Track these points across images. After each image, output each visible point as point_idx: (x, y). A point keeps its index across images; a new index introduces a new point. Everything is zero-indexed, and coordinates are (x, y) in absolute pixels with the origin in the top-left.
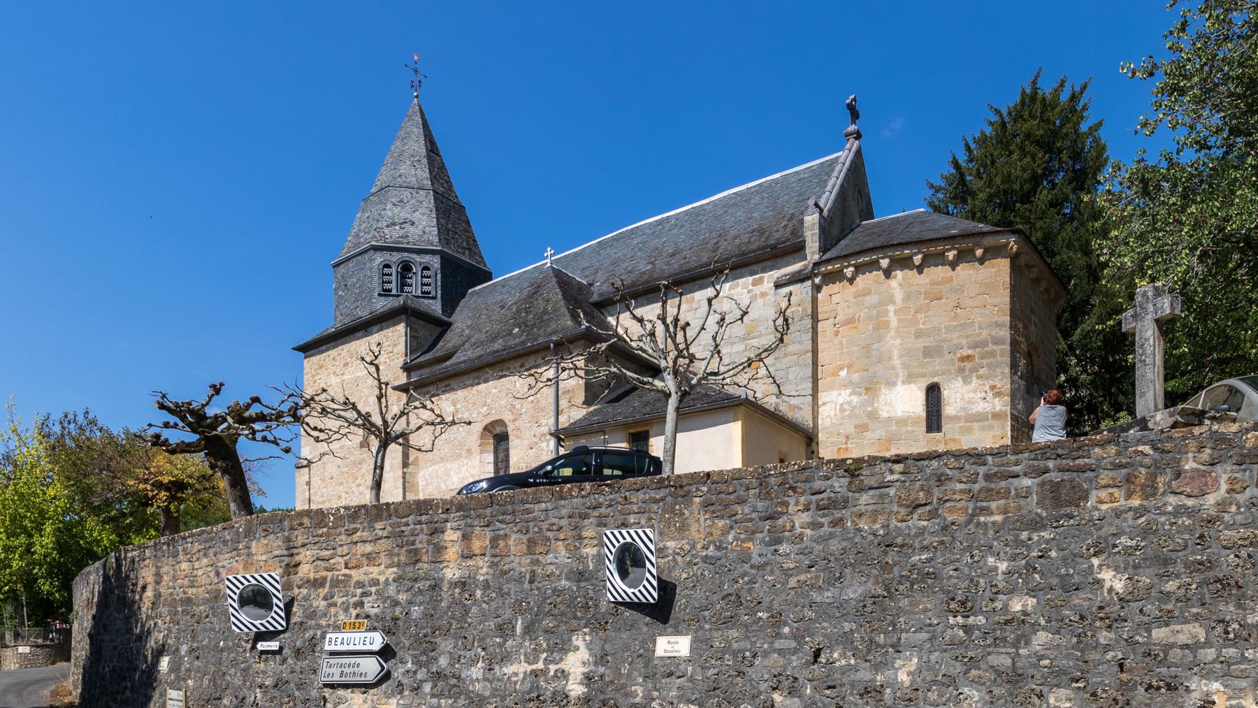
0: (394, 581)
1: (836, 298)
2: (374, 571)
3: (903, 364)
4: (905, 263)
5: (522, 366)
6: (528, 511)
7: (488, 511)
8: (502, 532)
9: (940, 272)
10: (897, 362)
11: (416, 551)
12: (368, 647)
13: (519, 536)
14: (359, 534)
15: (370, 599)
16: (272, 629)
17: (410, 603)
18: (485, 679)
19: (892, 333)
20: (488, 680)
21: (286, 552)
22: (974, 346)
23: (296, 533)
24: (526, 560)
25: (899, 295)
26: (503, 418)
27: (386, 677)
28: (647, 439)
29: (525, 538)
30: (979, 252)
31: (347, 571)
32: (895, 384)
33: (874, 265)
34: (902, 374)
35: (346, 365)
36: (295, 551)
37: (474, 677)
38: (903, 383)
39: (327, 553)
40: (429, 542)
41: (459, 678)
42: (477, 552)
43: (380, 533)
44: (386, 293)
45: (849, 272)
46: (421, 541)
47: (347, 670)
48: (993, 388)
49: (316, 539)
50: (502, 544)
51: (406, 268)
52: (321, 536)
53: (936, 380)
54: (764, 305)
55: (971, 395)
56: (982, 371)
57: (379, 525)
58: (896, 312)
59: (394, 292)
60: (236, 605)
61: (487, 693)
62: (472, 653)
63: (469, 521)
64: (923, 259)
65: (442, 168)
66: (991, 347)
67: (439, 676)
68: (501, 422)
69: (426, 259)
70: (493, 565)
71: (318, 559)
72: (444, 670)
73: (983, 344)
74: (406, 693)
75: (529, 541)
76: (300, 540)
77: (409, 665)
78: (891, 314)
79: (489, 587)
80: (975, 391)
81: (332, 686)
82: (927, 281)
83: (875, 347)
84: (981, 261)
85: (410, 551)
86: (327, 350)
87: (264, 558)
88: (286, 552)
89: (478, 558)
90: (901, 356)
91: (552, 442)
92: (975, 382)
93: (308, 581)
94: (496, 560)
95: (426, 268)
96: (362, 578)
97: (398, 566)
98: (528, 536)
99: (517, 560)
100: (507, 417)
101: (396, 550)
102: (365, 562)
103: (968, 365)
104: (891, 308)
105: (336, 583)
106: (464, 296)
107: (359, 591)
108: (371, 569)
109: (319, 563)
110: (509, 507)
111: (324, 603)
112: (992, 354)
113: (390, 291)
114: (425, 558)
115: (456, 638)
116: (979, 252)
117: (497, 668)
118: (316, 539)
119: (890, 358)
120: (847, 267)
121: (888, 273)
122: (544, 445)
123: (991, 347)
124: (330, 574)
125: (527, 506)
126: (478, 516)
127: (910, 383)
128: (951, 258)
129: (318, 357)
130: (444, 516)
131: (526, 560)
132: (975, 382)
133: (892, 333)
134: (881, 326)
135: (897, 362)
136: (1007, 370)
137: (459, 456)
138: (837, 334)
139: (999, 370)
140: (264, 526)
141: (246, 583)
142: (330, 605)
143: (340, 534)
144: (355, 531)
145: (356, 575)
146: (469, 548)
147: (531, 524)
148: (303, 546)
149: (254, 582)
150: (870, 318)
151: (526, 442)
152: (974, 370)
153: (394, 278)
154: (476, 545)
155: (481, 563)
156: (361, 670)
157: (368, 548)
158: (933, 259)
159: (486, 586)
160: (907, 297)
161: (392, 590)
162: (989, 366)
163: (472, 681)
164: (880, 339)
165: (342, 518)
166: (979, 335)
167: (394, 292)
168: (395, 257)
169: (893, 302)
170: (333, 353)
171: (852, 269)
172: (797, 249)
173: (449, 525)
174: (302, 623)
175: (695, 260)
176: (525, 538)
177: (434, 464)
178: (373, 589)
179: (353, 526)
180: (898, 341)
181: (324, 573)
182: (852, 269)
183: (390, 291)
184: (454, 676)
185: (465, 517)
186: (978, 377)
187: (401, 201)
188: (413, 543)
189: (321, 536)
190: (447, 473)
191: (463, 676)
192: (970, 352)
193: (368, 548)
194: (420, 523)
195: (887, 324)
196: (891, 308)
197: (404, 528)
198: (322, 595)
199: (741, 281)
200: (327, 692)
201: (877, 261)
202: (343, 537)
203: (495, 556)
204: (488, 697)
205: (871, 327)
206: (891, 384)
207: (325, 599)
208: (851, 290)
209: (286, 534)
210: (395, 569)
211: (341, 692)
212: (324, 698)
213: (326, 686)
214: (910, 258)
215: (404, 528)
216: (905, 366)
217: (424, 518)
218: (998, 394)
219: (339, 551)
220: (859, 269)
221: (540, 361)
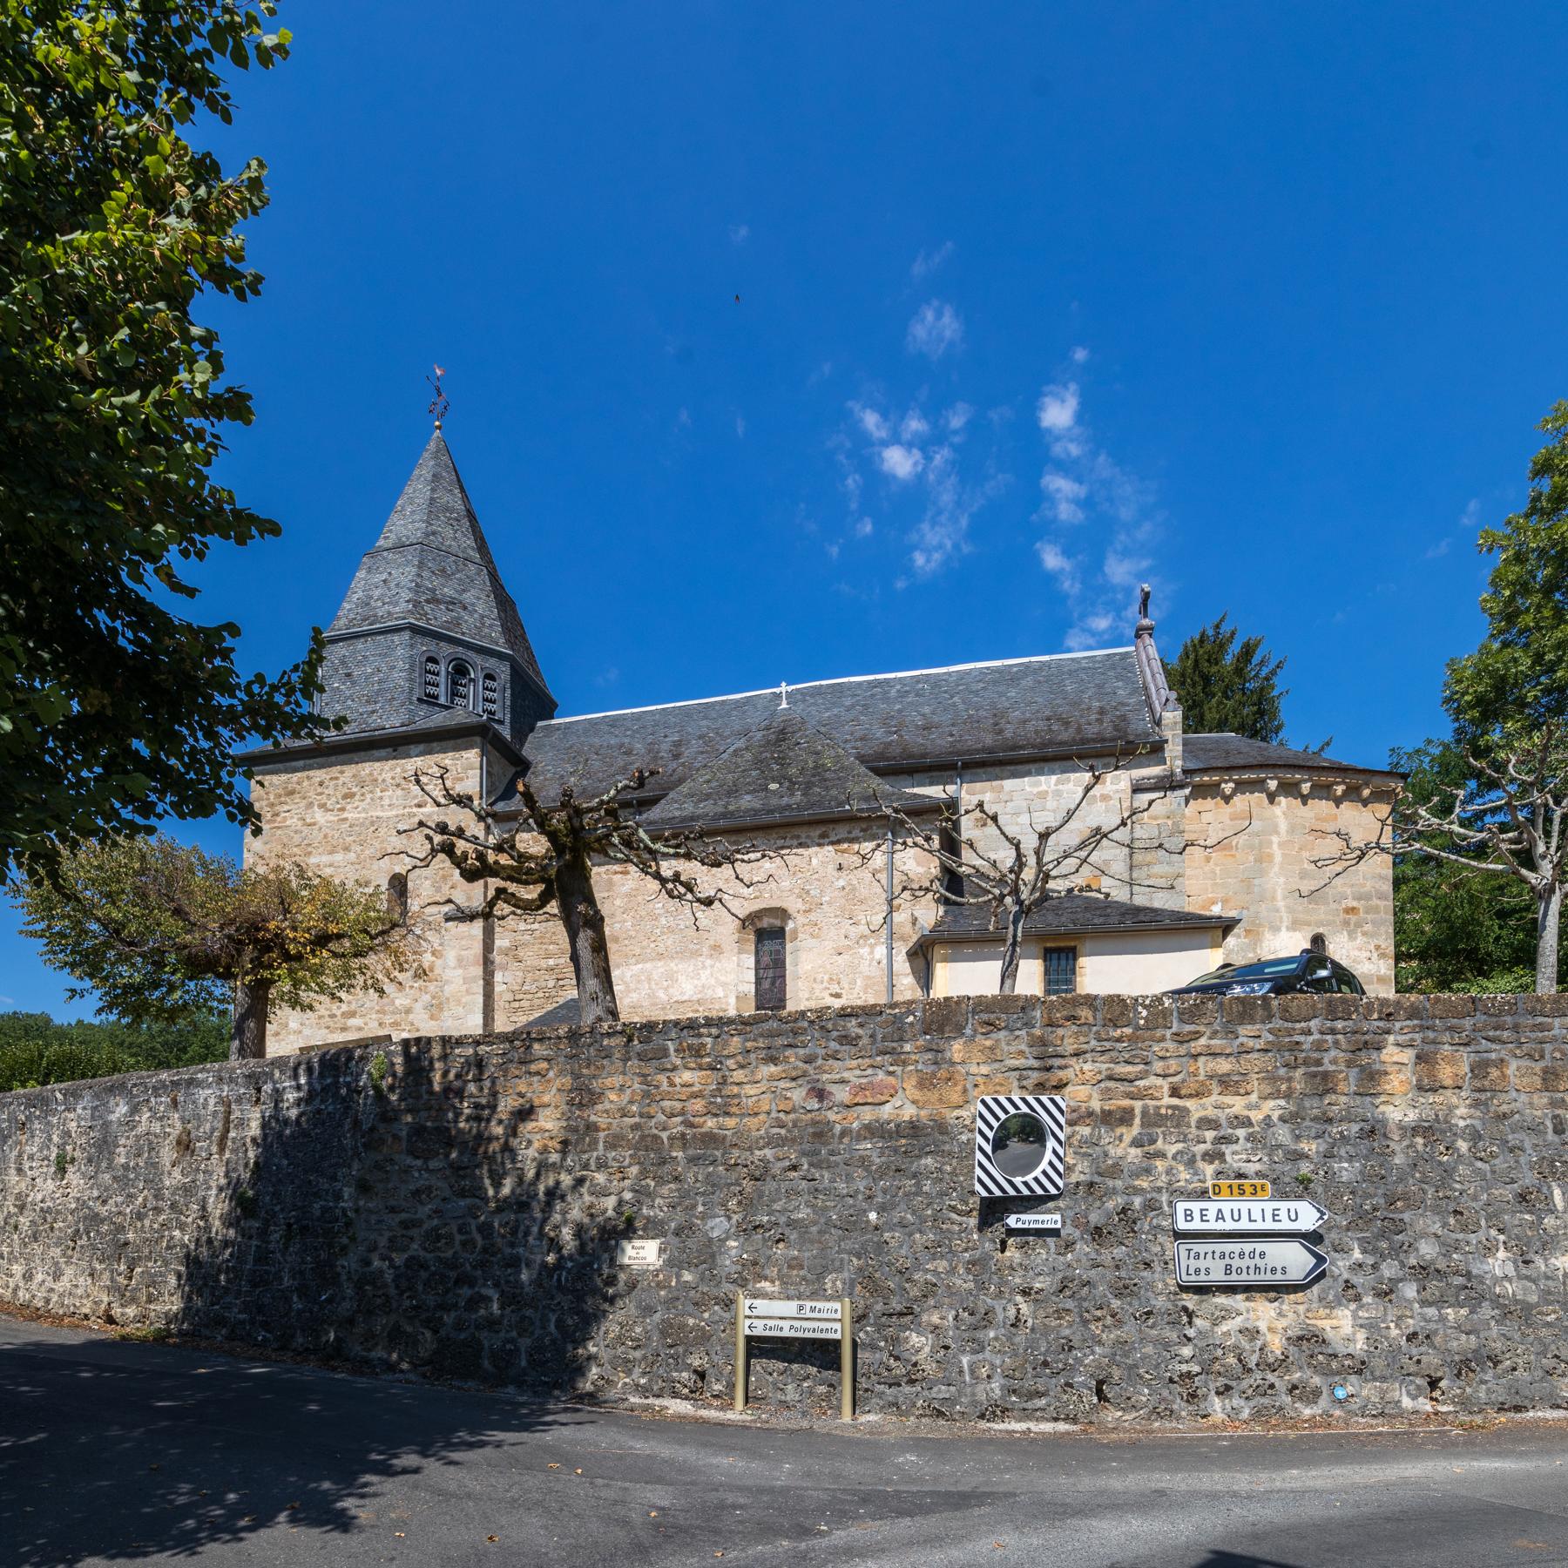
0: (1282, 1119)
1: (1206, 817)
2: (1237, 1105)
3: (1287, 907)
4: (1289, 789)
5: (823, 836)
6: (1542, 1028)
7: (1468, 1023)
8: (1493, 1056)
9: (1323, 807)
10: (1281, 904)
11: (1326, 1076)
12: (1286, 1225)
13: (1526, 1063)
14: (1203, 1041)
15: (1235, 1147)
16: (1040, 1192)
17: (1329, 1155)
18: (1520, 1277)
19: (1276, 869)
20: (1527, 1278)
21: (1036, 1063)
22: (1359, 899)
23: (1060, 1032)
24: (1542, 1100)
25: (1283, 826)
26: (784, 905)
27: (1318, 1276)
28: (1075, 959)
29: (1538, 1067)
30: (1366, 792)
31: (1175, 1101)
32: (1278, 929)
33: (1259, 785)
34: (1286, 919)
35: (349, 796)
36: (1057, 1062)
37: (1499, 1273)
38: (1288, 929)
39: (1129, 1068)
40: (1349, 1064)
41: (1468, 1275)
42: (1448, 1082)
43: (1251, 1043)
44: (430, 700)
45: (1228, 788)
46: (1333, 1060)
47: (1236, 1263)
48: (1378, 947)
49: (1108, 1045)
50: (1494, 1073)
51: (460, 670)
52: (1119, 1040)
53: (1321, 930)
54: (1107, 811)
55: (1357, 953)
56: (1367, 927)
57: (1245, 1030)
58: (1280, 845)
59: (442, 700)
60: (988, 1149)
61: (1534, 1299)
62: (1481, 1235)
63: (1431, 1035)
64: (1345, 793)
65: (482, 539)
66: (1375, 902)
67: (1423, 1272)
68: (783, 914)
69: (491, 663)
70: (1476, 1104)
71: (1110, 1078)
72: (1433, 1262)
73: (1367, 897)
74: (1368, 1299)
75: (1545, 1071)
76: (1069, 1046)
77: (1357, 1255)
78: (1275, 846)
79: (1480, 1137)
80: (1360, 949)
81: (1202, 1290)
82: (1311, 814)
83: (1256, 882)
84: (1365, 803)
85: (1314, 1075)
86: (310, 768)
87: (984, 1070)
88: (1036, 1063)
89: (1449, 1093)
90: (1285, 898)
91: (426, 965)
92: (1360, 939)
93: (1091, 1114)
94: (1483, 1097)
95: (490, 677)
96: (1211, 1113)
97: (1288, 1096)
98: (1542, 1064)
99: (1523, 1098)
100: (792, 904)
101: (1282, 1071)
102: (1216, 1089)
103: (1353, 918)
104: (1275, 839)
105: (1153, 1120)
106: (532, 729)
107: (1210, 1135)
108: (1228, 1100)
109: (1111, 1084)
110: (1508, 1019)
111: (1135, 1152)
112: (1376, 910)
113: (436, 697)
114: (1341, 1087)
115: (1437, 1210)
116: (1366, 792)
117: (1539, 1262)
118: (1108, 1045)
119: (1274, 898)
120: (1226, 782)
121: (1272, 798)
122: (864, 951)
123: (1375, 902)
124: (1138, 1105)
125: (1540, 1019)
126: (1451, 1029)
127: (1295, 930)
128: (1339, 793)
129: (284, 777)
130: (1381, 1024)
131: (1542, 1100)
132: (1360, 939)
133: (1276, 869)
134: (1263, 859)
135: (1281, 904)
136: (1391, 930)
137: (696, 954)
138: (1208, 860)
139: (1383, 929)
140: (985, 1017)
141: (1012, 1111)
142: (1149, 1156)
143: (1163, 1039)
144: (1197, 1035)
145: (1196, 1109)
146: (1432, 1076)
147: (1548, 1047)
148: (1076, 1055)
149: (1025, 1109)
150: (1252, 847)
151: (829, 945)
152: (1359, 925)
153: (442, 679)
154: (1446, 1073)
155: (1454, 1100)
156: (1270, 1261)
157: (1224, 1066)
158: (1322, 791)
159: (1475, 1137)
160: (1292, 829)
161: (1283, 1134)
162: (1374, 922)
163: (1497, 1281)
164: (1262, 873)
165: (1165, 1014)
166: (1363, 886)
167: (442, 700)
168: (446, 650)
169: (1278, 833)
170: (319, 775)
171: (1232, 785)
172: (1157, 750)
173: (1391, 1038)
174: (1091, 1184)
175: (939, 743)
176: (1538, 1067)
177: (644, 961)
178: (1241, 1133)
179: (1188, 1028)
180: (1282, 880)
181: (1126, 1103)
182: (1232, 785)
183: (436, 697)
184: (1457, 1273)
185: (1423, 1028)
186: (1364, 934)
187: (443, 571)
188: (1319, 1063)
189: (1119, 1040)
190: (671, 977)
191: (1475, 1272)
192: (1355, 904)
193: (1224, 1066)
194: (1333, 1031)
195: (1270, 857)
196: (1275, 839)
197: (1301, 1038)
198: (1127, 1139)
199: (1073, 776)
200: (1190, 1301)
201: (1263, 781)
202: (1170, 1045)
203: (1479, 1090)
204: (1537, 1305)
205: (1251, 858)
206: (1276, 929)
207: (1136, 1143)
208: (1226, 810)
209: (1037, 1032)
210: (1282, 1102)
211: (1221, 1300)
212: (1185, 1309)
213: (1184, 1289)
214: (1297, 784)
215: (1301, 1038)
216: (1290, 910)
217: (1339, 1025)
218: (1382, 956)
219: (1158, 1066)
220: (1241, 787)
221: (856, 833)
